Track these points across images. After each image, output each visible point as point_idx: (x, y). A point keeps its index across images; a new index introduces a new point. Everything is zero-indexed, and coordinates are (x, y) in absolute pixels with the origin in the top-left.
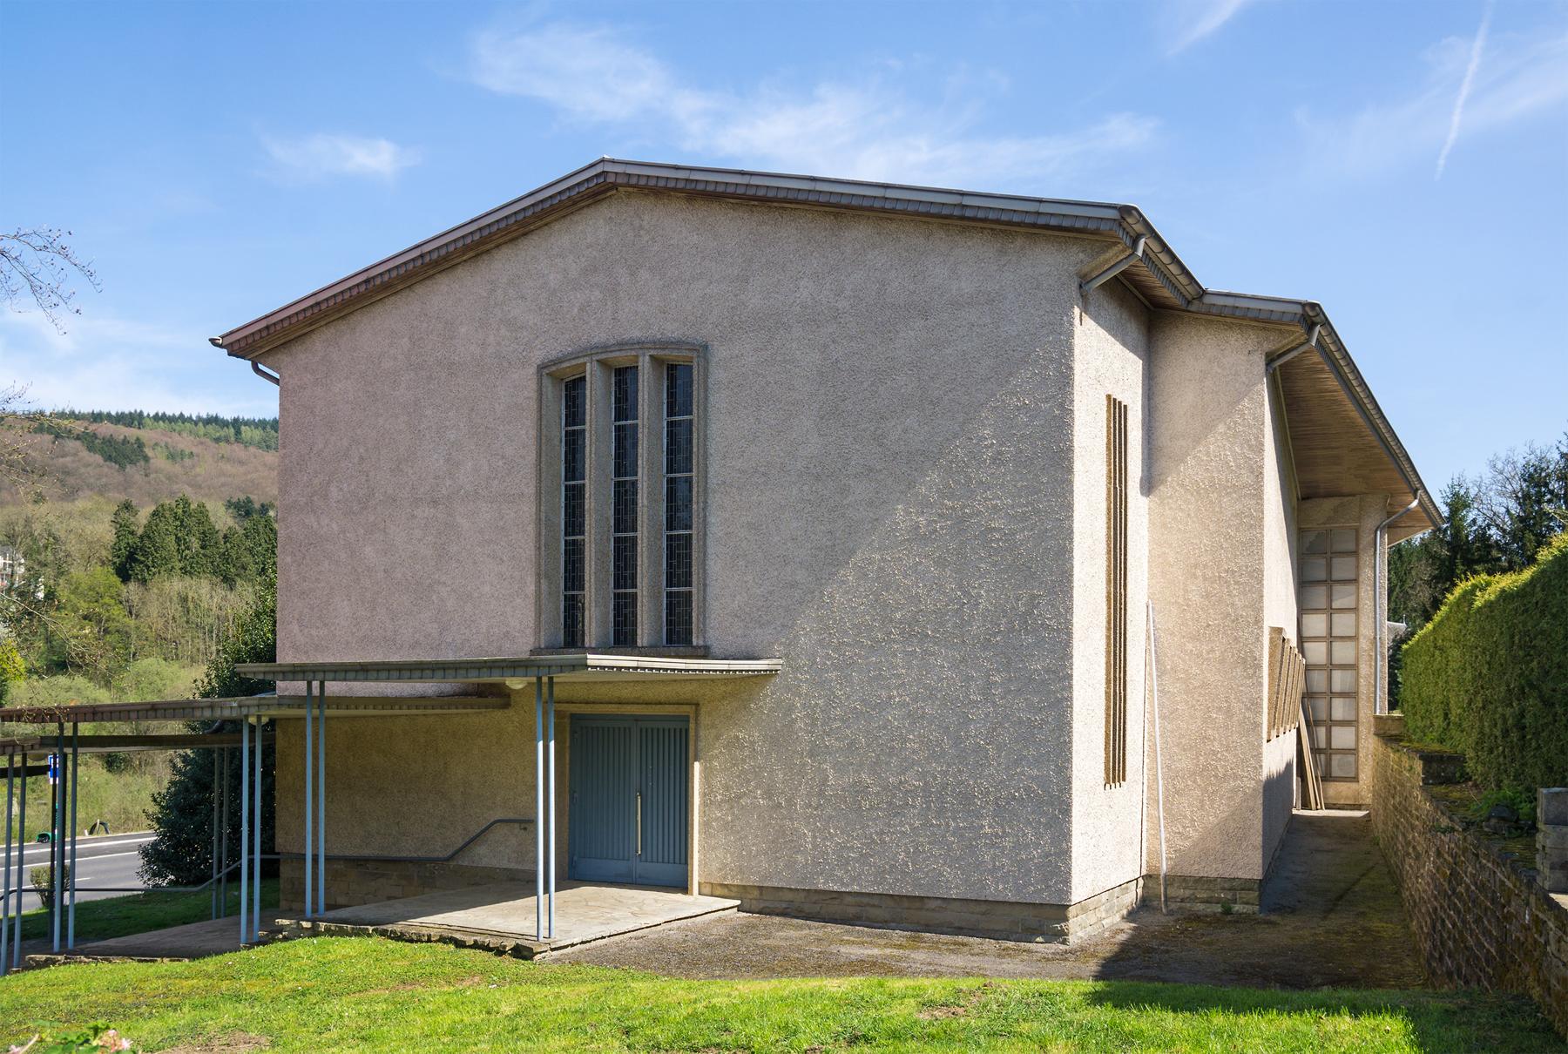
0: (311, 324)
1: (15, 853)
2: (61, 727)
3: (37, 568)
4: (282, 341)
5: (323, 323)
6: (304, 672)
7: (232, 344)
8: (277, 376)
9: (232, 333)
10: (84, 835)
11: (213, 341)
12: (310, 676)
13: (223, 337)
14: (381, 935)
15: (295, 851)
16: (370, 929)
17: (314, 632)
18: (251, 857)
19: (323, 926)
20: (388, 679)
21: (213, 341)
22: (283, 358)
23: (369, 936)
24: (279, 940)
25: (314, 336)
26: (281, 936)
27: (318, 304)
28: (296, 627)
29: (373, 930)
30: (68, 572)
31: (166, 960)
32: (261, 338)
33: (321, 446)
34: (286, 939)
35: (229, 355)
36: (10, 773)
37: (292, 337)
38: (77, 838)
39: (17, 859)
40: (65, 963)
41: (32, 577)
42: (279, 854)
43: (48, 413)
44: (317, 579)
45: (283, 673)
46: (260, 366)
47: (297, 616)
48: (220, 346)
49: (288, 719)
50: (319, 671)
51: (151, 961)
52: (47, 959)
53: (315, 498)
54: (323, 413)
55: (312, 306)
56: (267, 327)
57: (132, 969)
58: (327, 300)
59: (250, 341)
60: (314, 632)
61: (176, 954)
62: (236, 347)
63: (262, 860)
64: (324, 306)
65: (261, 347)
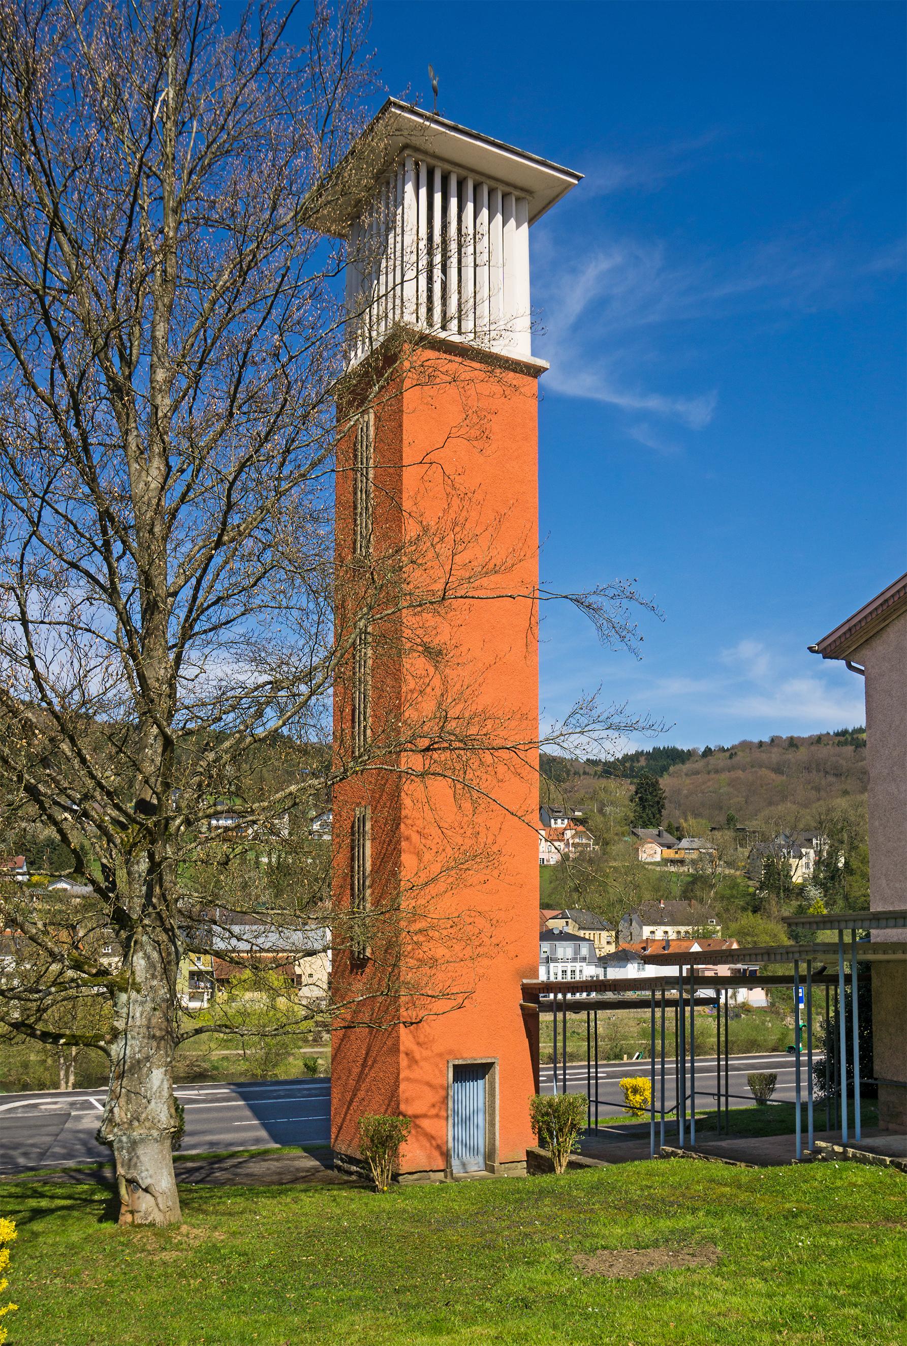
0: (884, 620)
1: (658, 1067)
2: (797, 967)
3: (836, 845)
4: (864, 639)
5: (894, 617)
6: (831, 922)
7: (825, 649)
8: (863, 668)
9: (824, 639)
10: (622, 1059)
11: (811, 649)
12: (843, 925)
13: (818, 644)
14: (897, 1167)
15: (889, 1078)
16: (888, 1159)
17: (897, 885)
18: (850, 1080)
19: (850, 1151)
20: (895, 926)
21: (811, 649)
22: (866, 653)
23: (886, 1166)
24: (819, 1160)
25: (888, 630)
26: (820, 1157)
27: (886, 601)
28: (884, 881)
29: (890, 1162)
30: (857, 847)
31: (743, 1165)
32: (846, 639)
33: (898, 723)
34: (824, 1159)
35: (824, 658)
36: (692, 1002)
37: (872, 634)
38: (567, 1065)
39: (660, 1071)
40: (682, 1157)
41: (833, 854)
42: (876, 1079)
43: (832, 733)
44: (899, 839)
45: (816, 923)
46: (853, 664)
47: (884, 872)
48: (817, 652)
49: (881, 962)
50: (850, 920)
51: (732, 1164)
52: (673, 1151)
53: (895, 768)
54: (898, 694)
55: (881, 605)
56: (850, 629)
57: (718, 1168)
58: (893, 596)
59: (838, 643)
60: (897, 885)
61: (751, 1160)
62: (828, 650)
63: (861, 1084)
64: (891, 602)
65: (849, 647)
